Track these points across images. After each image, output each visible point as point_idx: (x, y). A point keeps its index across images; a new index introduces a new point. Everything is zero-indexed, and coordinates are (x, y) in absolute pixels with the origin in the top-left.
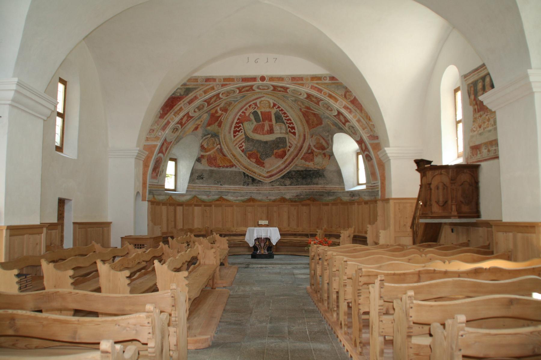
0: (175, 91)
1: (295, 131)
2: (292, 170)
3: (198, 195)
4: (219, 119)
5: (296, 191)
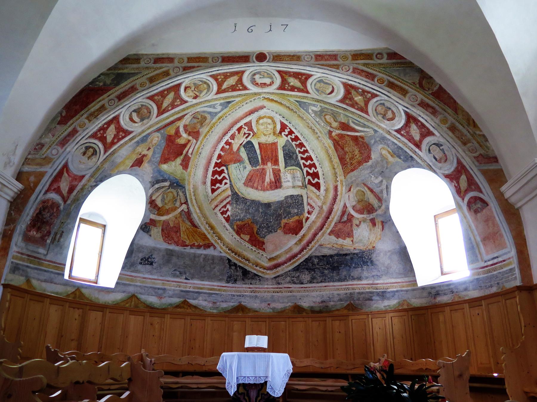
0: (95, 78)
1: (318, 181)
2: (314, 254)
3: (141, 293)
4: (184, 152)
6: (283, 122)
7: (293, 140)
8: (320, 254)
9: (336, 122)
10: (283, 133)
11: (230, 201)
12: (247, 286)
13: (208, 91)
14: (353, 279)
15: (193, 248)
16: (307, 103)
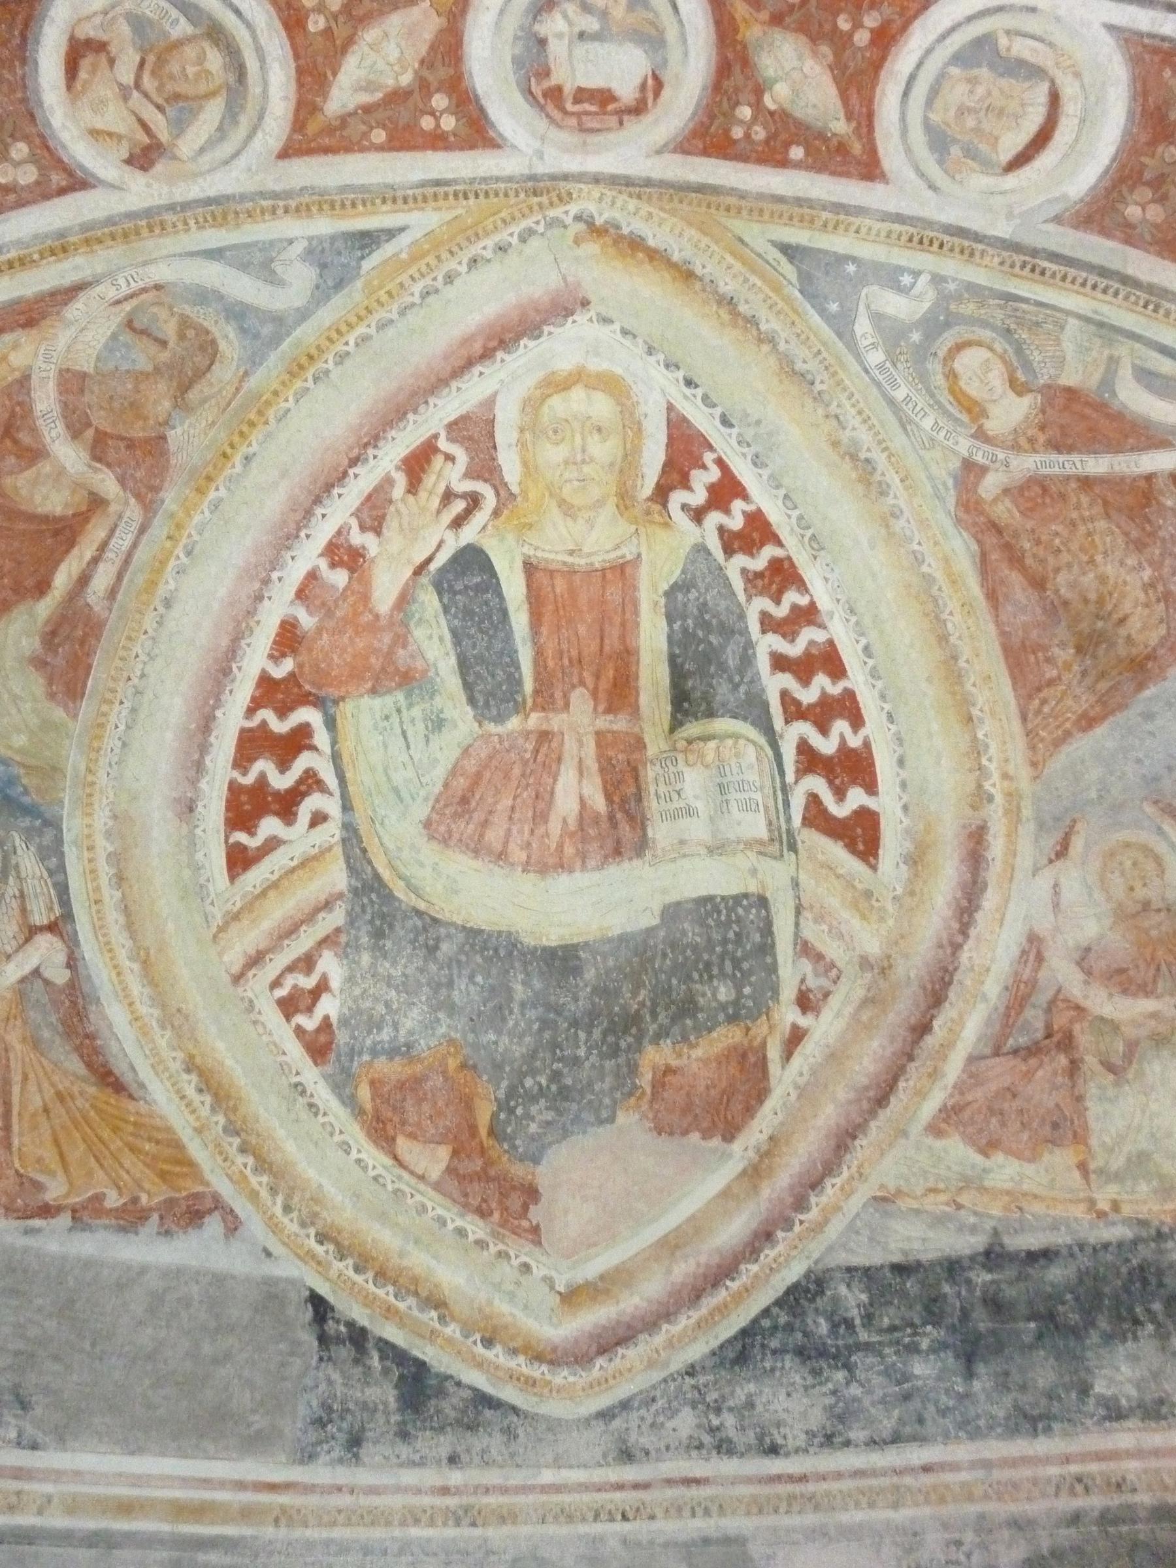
1: (871, 803)
2: (842, 1258)
4: (63, 578)
5: (477, 1532)
6: (685, 420)
7: (733, 543)
8: (874, 1257)
9: (1018, 388)
10: (678, 498)
11: (338, 930)
12: (430, 1477)
13: (232, 113)
14: (1109, 1418)
15: (87, 1228)
16: (854, 259)
